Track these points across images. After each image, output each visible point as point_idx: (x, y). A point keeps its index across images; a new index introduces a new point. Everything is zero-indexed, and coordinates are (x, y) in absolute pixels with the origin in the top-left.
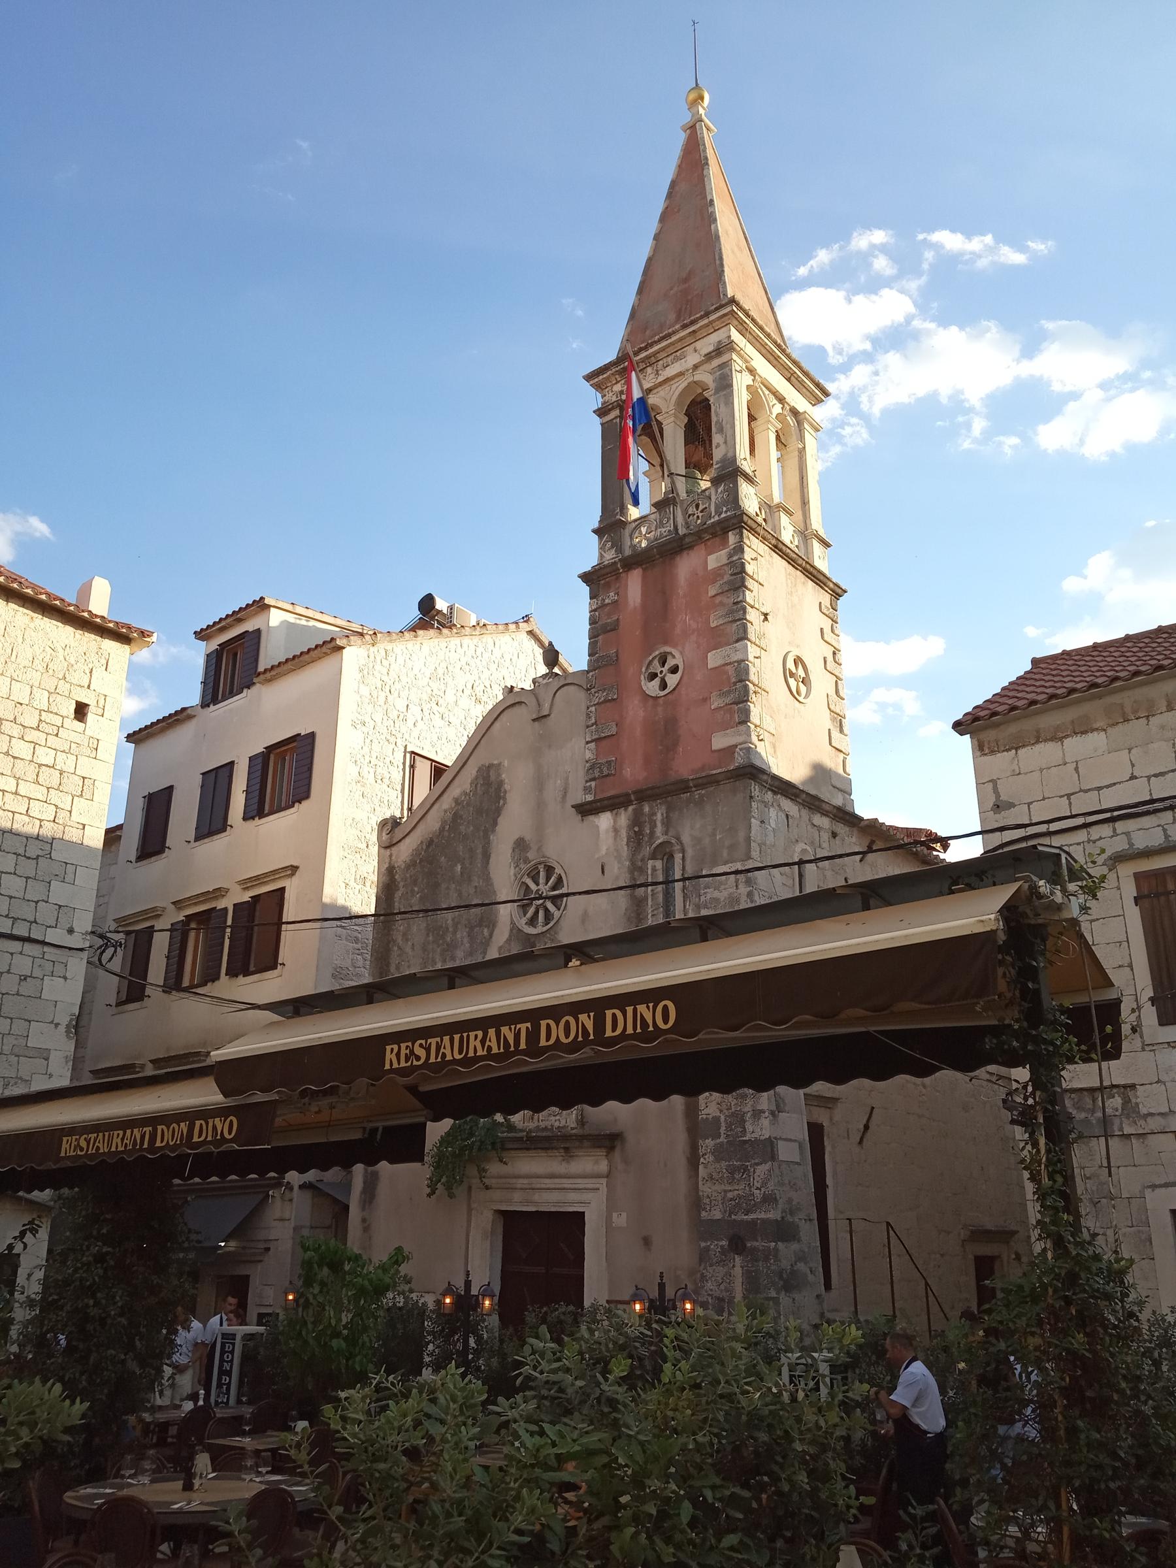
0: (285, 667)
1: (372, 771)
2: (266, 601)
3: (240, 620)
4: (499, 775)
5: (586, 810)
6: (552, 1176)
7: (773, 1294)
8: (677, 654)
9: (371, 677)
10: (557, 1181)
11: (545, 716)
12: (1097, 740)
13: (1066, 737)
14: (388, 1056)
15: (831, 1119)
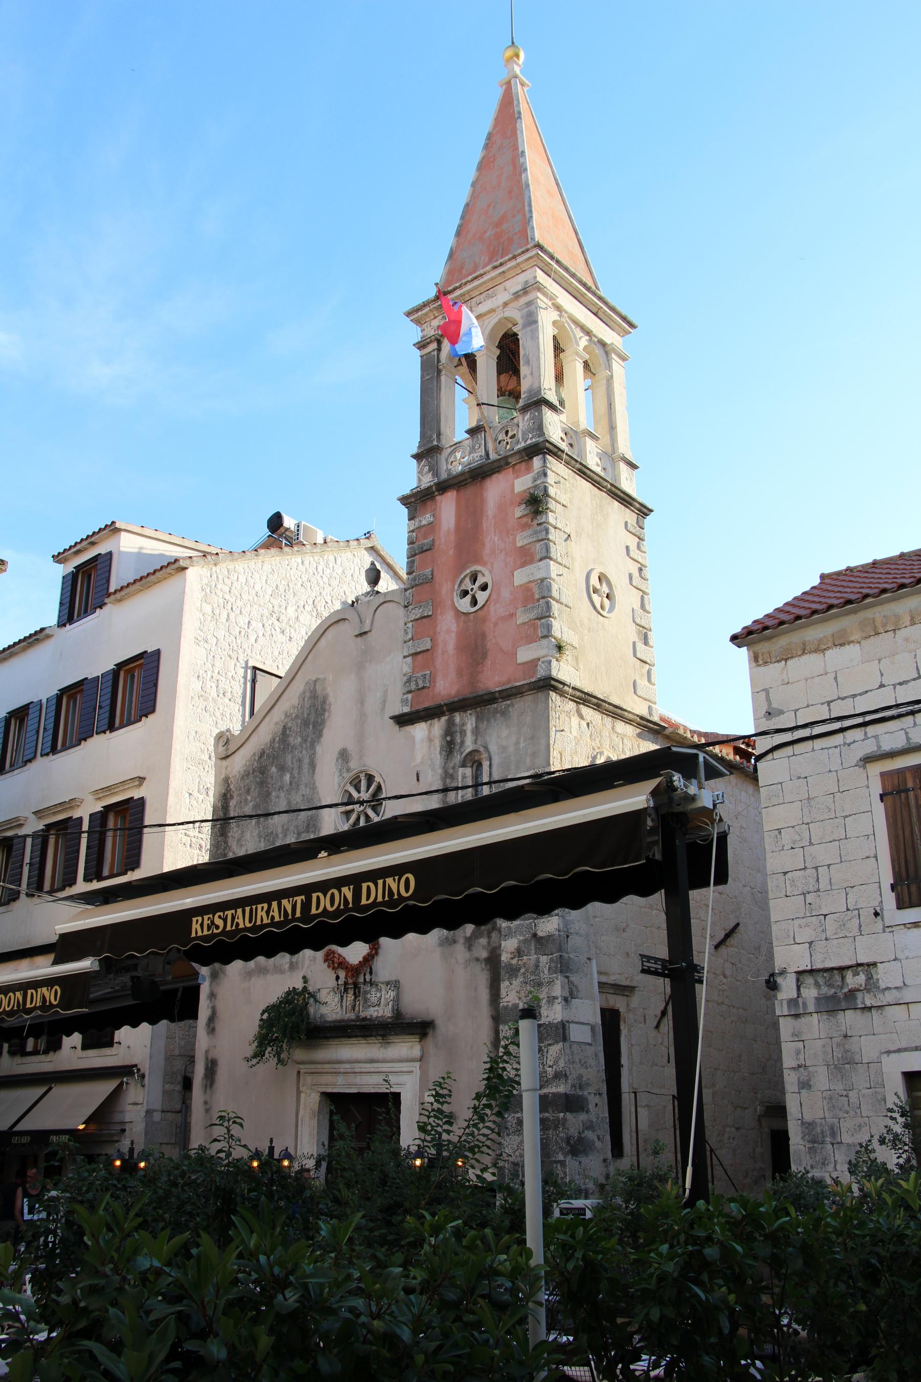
0: (132, 588)
1: (214, 685)
2: (117, 525)
3: (93, 544)
4: (324, 689)
5: (402, 720)
6: (372, 1061)
7: (561, 1157)
8: (487, 573)
9: (213, 595)
10: (375, 1065)
11: (365, 633)
12: (852, 651)
13: (828, 648)
14: (194, 926)
15: (628, 1005)
